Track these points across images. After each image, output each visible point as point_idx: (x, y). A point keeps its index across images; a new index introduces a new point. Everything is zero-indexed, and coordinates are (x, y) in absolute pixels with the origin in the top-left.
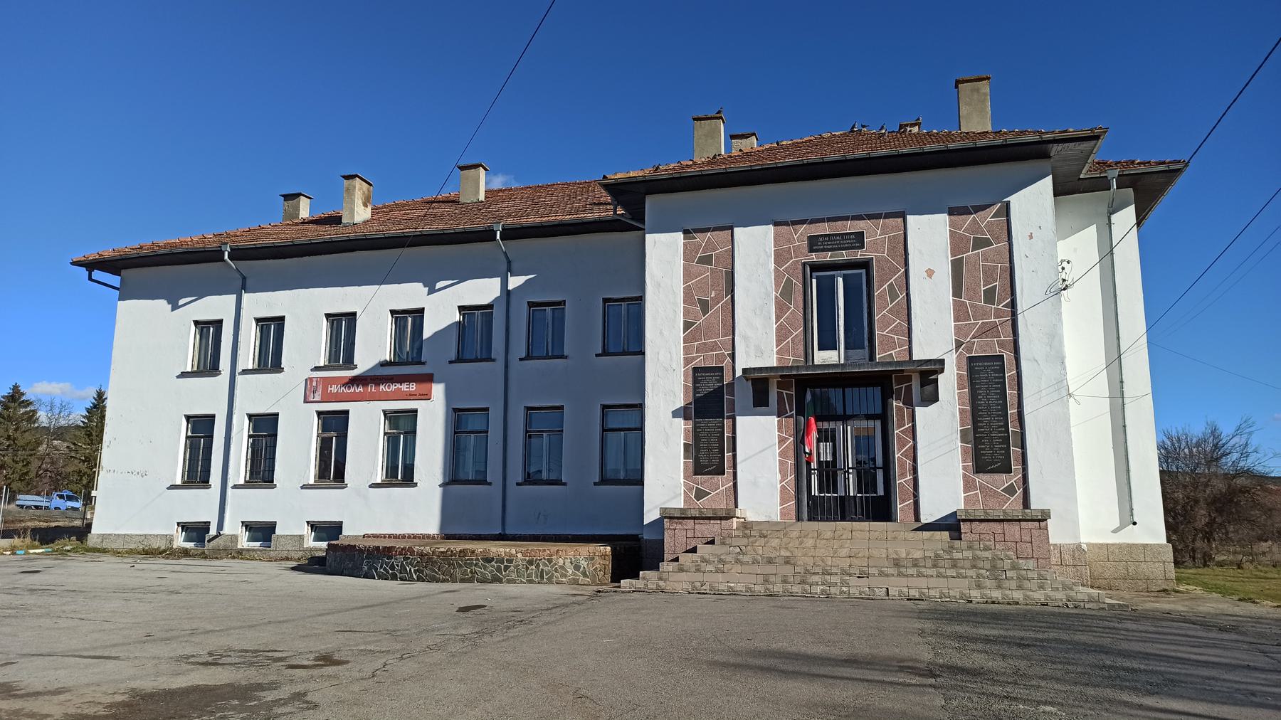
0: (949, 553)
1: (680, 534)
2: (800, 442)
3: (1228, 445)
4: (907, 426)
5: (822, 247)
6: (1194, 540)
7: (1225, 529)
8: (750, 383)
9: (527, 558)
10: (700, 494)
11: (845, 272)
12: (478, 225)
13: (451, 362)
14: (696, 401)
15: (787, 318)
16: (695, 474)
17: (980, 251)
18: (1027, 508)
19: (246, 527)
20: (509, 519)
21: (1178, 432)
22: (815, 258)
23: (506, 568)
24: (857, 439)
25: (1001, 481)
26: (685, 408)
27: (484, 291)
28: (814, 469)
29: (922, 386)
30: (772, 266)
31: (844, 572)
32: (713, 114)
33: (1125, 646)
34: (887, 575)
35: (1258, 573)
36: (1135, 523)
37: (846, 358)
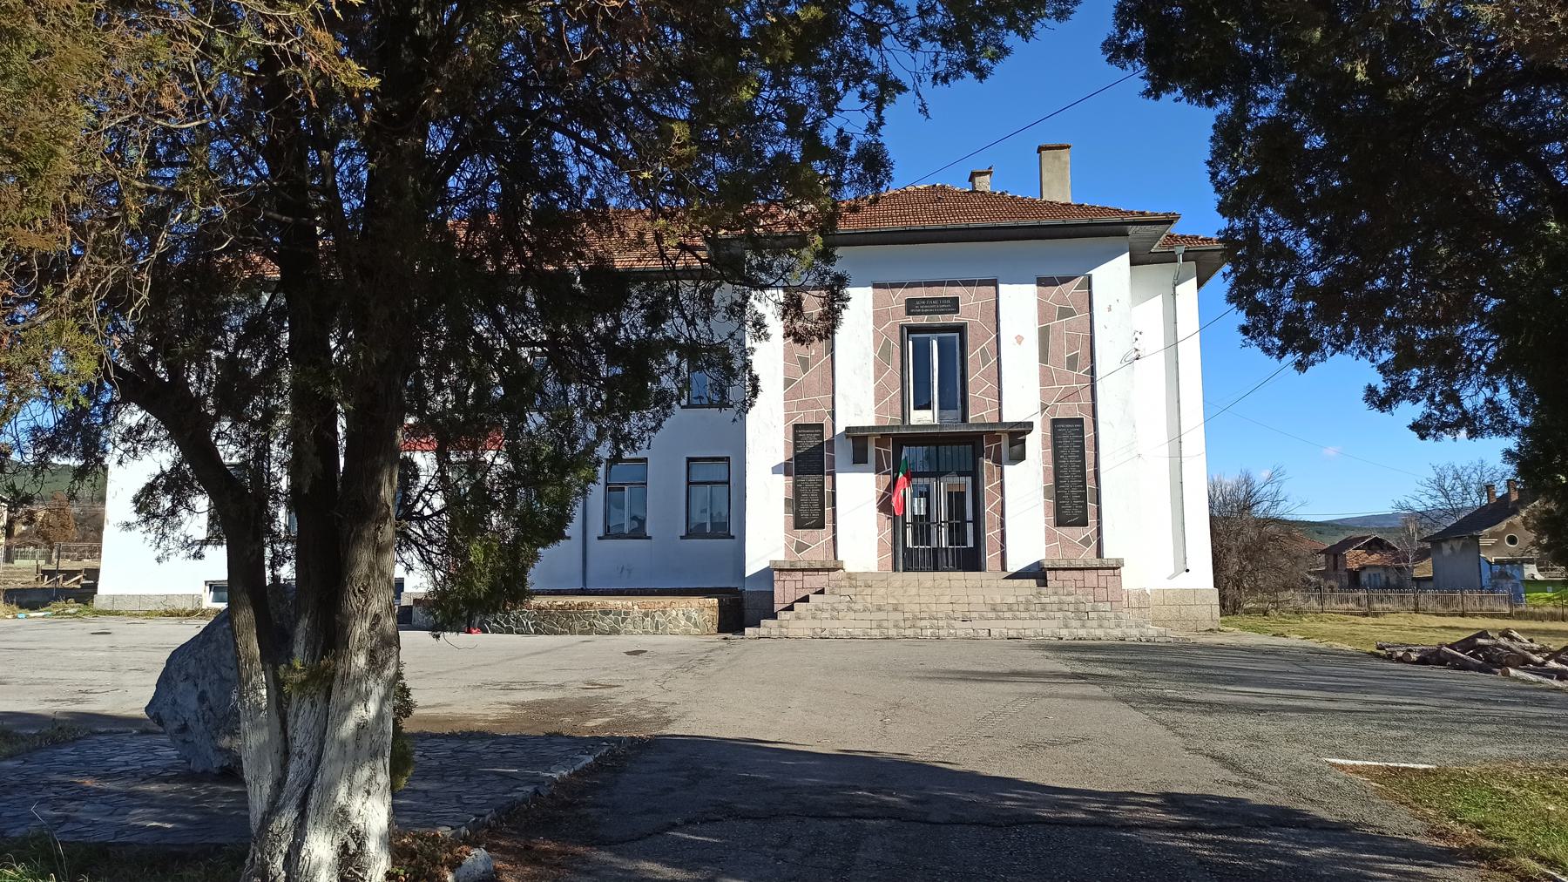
1: (790, 586)
10: (801, 547)
14: (797, 457)
20: (591, 574)
22: (912, 320)
23: (624, 620)
25: (1078, 533)
26: (786, 464)
30: (871, 326)
31: (948, 617)
33: (1200, 663)
36: (1187, 571)
37: (940, 418)
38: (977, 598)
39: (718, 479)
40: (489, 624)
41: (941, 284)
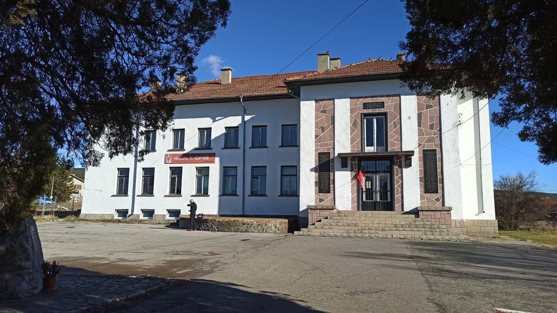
0: (415, 222)
2: (359, 182)
3: (526, 181)
4: (399, 175)
5: (368, 107)
6: (511, 220)
7: (523, 215)
8: (340, 159)
9: (258, 223)
10: (321, 200)
11: (377, 117)
12: (233, 95)
13: (222, 149)
14: (320, 165)
15: (355, 134)
16: (319, 193)
17: (428, 110)
18: (444, 206)
19: (142, 211)
21: (506, 176)
22: (365, 111)
23: (250, 227)
24: (381, 180)
25: (434, 196)
27: (235, 121)
28: (364, 191)
29: (406, 160)
30: (349, 114)
31: (376, 229)
32: (325, 53)
33: (475, 252)
34: (392, 230)
35: (535, 233)
36: (484, 212)
37: (377, 150)
38: (389, 222)
39: (293, 174)
40: (201, 227)
41: (377, 96)
